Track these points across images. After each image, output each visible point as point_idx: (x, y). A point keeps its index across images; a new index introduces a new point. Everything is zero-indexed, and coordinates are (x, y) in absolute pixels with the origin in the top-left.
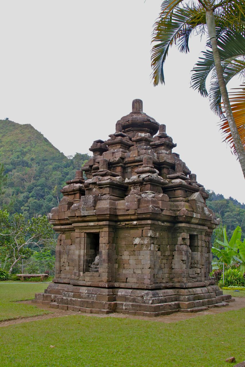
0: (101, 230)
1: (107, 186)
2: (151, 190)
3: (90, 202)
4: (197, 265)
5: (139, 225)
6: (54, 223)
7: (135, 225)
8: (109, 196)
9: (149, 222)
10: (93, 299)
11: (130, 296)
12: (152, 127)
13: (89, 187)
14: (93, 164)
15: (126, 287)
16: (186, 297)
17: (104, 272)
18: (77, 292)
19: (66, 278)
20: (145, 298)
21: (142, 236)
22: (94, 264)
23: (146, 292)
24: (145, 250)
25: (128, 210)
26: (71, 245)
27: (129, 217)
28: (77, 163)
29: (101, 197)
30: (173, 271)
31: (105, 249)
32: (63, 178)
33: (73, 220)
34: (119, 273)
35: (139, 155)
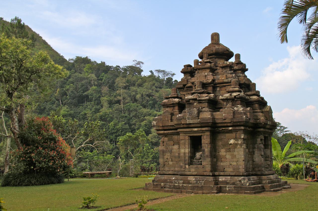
0: (203, 134)
1: (206, 101)
2: (241, 105)
3: (195, 113)
4: (268, 159)
5: (234, 130)
6: (158, 128)
7: (230, 130)
8: (208, 109)
9: (242, 128)
10: (201, 184)
11: (230, 181)
12: (228, 54)
13: (189, 102)
14: (186, 83)
15: (225, 175)
16: (267, 181)
17: (207, 165)
18: (186, 180)
19: (170, 171)
20: (242, 182)
21: (236, 138)
22: (196, 159)
23: (243, 177)
24: (239, 148)
25: (225, 119)
26: (174, 145)
27: (226, 125)
28: (78, 67)
29: (202, 109)
30: (254, 163)
31: (207, 148)
32: (65, 81)
33: (179, 126)
34: (218, 165)
35: (227, 78)
